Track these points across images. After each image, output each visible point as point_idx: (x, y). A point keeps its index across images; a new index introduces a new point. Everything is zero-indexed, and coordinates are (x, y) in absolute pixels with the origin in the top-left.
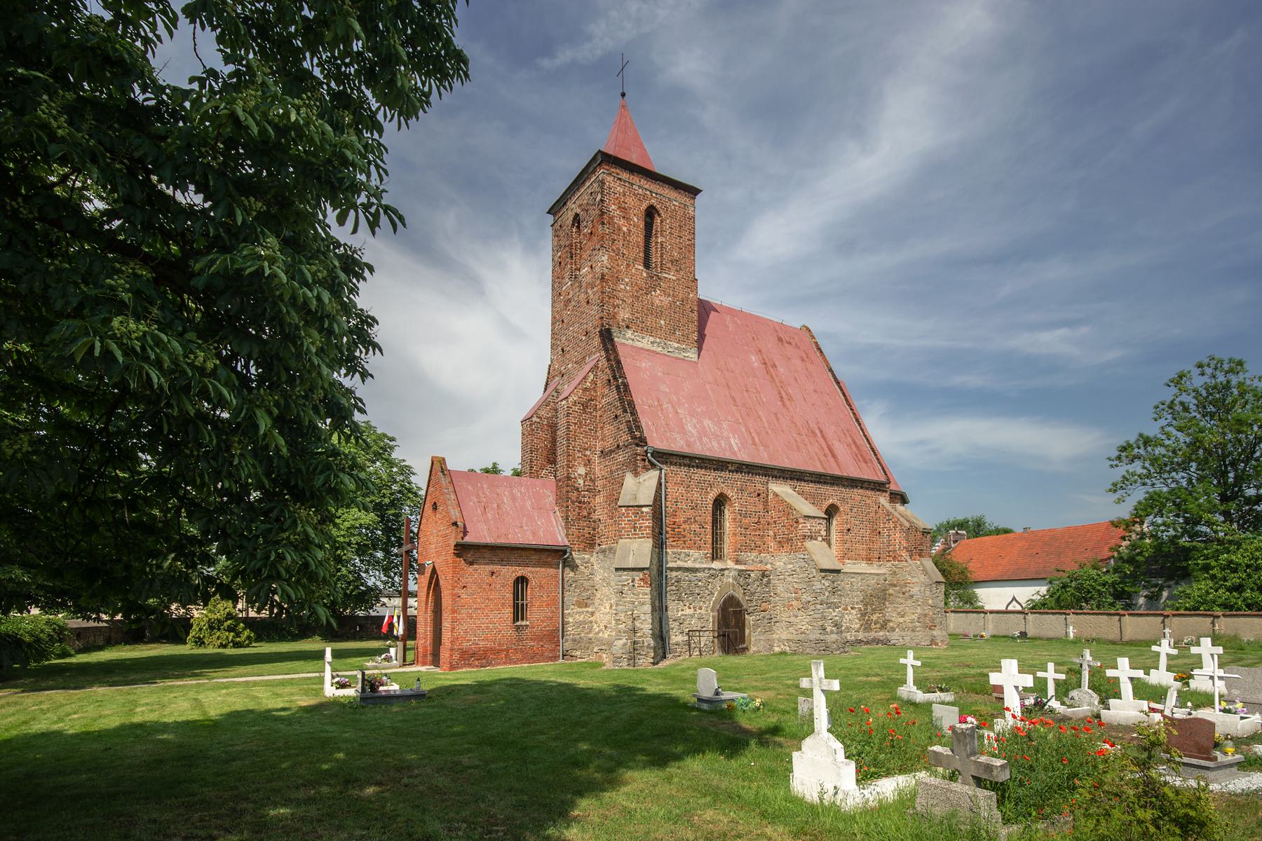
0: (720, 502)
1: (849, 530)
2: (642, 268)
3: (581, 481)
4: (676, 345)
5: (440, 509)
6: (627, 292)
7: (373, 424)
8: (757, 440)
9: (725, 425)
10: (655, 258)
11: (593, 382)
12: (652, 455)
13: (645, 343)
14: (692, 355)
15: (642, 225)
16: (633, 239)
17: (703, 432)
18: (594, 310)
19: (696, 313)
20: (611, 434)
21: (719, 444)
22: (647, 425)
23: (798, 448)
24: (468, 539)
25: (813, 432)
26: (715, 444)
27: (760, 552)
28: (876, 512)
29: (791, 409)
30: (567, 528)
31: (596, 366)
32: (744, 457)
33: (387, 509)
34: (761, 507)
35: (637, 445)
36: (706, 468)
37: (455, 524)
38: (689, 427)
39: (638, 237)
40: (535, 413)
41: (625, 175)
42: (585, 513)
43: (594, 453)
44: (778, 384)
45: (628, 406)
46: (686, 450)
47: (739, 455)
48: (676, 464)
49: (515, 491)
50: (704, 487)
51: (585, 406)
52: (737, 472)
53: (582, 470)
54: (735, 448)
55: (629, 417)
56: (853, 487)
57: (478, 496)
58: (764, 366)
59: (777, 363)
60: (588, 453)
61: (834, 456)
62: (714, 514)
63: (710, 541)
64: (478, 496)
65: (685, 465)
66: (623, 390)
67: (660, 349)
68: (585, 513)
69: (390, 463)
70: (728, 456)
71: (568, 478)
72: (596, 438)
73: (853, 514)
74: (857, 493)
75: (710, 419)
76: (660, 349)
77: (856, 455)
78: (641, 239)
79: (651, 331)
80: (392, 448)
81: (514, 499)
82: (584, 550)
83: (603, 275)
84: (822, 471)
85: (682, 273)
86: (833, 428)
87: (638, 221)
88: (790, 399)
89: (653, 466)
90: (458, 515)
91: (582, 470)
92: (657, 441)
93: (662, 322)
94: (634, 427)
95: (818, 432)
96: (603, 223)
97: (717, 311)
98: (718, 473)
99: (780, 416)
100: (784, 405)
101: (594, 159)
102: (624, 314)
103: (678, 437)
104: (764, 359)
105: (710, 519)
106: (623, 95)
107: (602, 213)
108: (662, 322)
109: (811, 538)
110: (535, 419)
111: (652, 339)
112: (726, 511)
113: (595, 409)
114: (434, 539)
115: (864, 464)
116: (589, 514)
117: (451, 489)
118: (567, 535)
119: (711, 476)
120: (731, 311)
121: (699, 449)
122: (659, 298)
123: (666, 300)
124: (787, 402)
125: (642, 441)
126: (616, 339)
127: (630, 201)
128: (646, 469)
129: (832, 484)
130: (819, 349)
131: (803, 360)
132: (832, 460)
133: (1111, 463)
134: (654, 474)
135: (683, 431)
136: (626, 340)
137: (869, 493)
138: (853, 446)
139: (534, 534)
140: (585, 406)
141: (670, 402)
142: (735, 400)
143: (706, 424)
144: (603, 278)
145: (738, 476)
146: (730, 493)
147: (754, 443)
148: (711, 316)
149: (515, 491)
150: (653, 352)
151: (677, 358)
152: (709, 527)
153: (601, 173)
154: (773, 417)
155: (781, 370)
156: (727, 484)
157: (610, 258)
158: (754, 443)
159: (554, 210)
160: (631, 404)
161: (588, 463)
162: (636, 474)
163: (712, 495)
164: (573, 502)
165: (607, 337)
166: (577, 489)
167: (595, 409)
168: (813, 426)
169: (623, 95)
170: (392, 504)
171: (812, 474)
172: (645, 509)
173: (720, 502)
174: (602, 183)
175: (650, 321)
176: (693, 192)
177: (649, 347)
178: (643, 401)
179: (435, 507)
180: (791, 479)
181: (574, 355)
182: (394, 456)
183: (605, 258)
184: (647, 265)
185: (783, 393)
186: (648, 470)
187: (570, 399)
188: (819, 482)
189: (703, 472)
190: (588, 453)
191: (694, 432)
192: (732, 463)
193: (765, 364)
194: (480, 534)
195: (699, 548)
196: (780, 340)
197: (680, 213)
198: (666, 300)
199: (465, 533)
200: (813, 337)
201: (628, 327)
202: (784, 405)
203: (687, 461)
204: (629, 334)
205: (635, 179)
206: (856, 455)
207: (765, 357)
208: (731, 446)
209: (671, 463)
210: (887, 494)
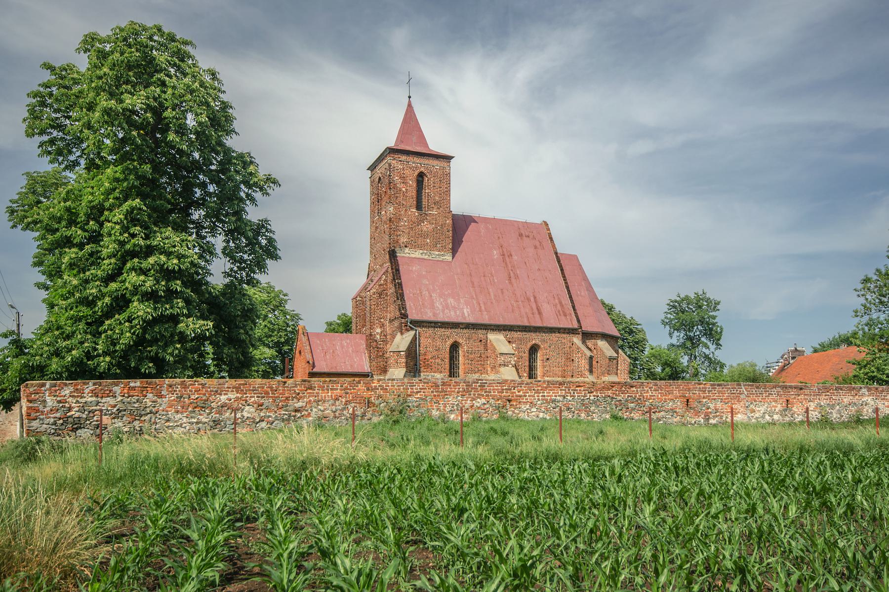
0: (455, 347)
1: (548, 359)
2: (414, 210)
3: (378, 336)
4: (437, 253)
5: (302, 354)
6: (405, 226)
7: (272, 284)
8: (483, 308)
9: (462, 301)
10: (424, 202)
11: (386, 280)
12: (411, 323)
13: (417, 254)
14: (448, 257)
15: (415, 185)
16: (409, 194)
17: (447, 306)
18: (387, 238)
19: (451, 232)
20: (392, 311)
21: (455, 313)
22: (410, 306)
23: (513, 311)
24: (315, 370)
25: (529, 300)
26: (452, 313)
27: (481, 374)
28: (570, 347)
29: (515, 285)
30: (370, 362)
31: (387, 271)
32: (471, 320)
33: (283, 346)
34: (482, 348)
35: (402, 318)
36: (445, 328)
37: (308, 362)
38: (437, 304)
39: (413, 193)
40: (359, 295)
41: (404, 158)
42: (381, 354)
43: (386, 320)
44: (510, 268)
45: (400, 296)
46: (433, 319)
47: (467, 319)
48: (426, 327)
49: (344, 342)
50: (444, 339)
51: (380, 294)
52: (466, 328)
53: (379, 330)
54: (467, 315)
55: (399, 302)
56: (551, 332)
57: (322, 346)
58: (501, 257)
59: (513, 253)
60: (382, 320)
61: (540, 313)
62: (451, 352)
63: (448, 368)
64: (322, 346)
65: (432, 327)
66: (399, 286)
67: (427, 257)
68: (381, 354)
69: (285, 313)
70: (460, 320)
71: (371, 335)
72: (387, 312)
73: (551, 349)
74: (554, 337)
75: (452, 298)
76: (427, 257)
77: (559, 311)
78: (414, 194)
79: (421, 247)
80: (286, 301)
81: (342, 347)
82: (380, 374)
83: (390, 219)
84: (527, 324)
85: (441, 209)
86: (546, 294)
87: (412, 183)
88: (517, 277)
89: (412, 329)
90: (311, 357)
91: (379, 330)
92: (414, 314)
93: (428, 241)
94: (402, 307)
95: (532, 299)
96: (390, 189)
97: (475, 222)
98: (453, 330)
99: (505, 291)
100: (510, 283)
101: (385, 150)
102: (403, 240)
103: (428, 311)
104: (503, 252)
105: (447, 356)
106: (410, 97)
107: (390, 183)
108: (428, 241)
109: (505, 365)
110: (358, 298)
111: (421, 251)
112: (460, 352)
113: (387, 296)
114: (300, 370)
115: (563, 318)
116: (383, 354)
117: (308, 343)
118: (370, 366)
119: (448, 332)
120: (486, 220)
121: (441, 318)
122: (426, 227)
123: (431, 227)
124: (513, 280)
125: (405, 316)
126: (398, 255)
127: (407, 172)
128: (407, 330)
129: (535, 332)
130: (551, 239)
131: (536, 247)
132: (537, 316)
133: (858, 293)
134: (412, 333)
135: (433, 306)
136: (404, 254)
137: (564, 336)
138: (559, 306)
139: (351, 366)
140: (380, 294)
141: (428, 290)
142: (473, 284)
143: (449, 302)
144: (390, 220)
145: (465, 331)
146: (461, 341)
147: (480, 310)
148: (470, 228)
149: (344, 342)
150: (422, 259)
151: (438, 261)
152: (447, 361)
153: (389, 159)
154: (499, 292)
155: (515, 258)
156: (535, 339)
157: (395, 208)
158: (480, 310)
159: (372, 168)
160: (402, 295)
161: (382, 326)
162: (402, 334)
163: (449, 343)
164: (373, 348)
165: (392, 254)
166: (376, 341)
167: (387, 296)
168: (530, 294)
169: (410, 97)
170: (287, 342)
171: (519, 326)
172: (402, 353)
173: (455, 347)
174: (390, 165)
175: (420, 241)
176: (448, 158)
177: (420, 256)
178: (410, 292)
179: (300, 352)
180: (504, 330)
181: (380, 261)
182: (287, 307)
183: (391, 209)
184: (419, 207)
185: (512, 274)
186: (408, 331)
187: (372, 291)
188: (525, 331)
189: (443, 330)
190: (382, 320)
191: (440, 307)
192: (462, 324)
193: (503, 255)
194: (321, 367)
195: (441, 372)
196: (521, 235)
197: (440, 172)
198: (431, 227)
199: (314, 366)
200: (549, 229)
201: (406, 247)
202: (510, 283)
203: (433, 325)
204: (407, 250)
205: (410, 158)
206: (559, 311)
207: (505, 250)
208: (463, 313)
209: (423, 327)
210: (580, 336)
